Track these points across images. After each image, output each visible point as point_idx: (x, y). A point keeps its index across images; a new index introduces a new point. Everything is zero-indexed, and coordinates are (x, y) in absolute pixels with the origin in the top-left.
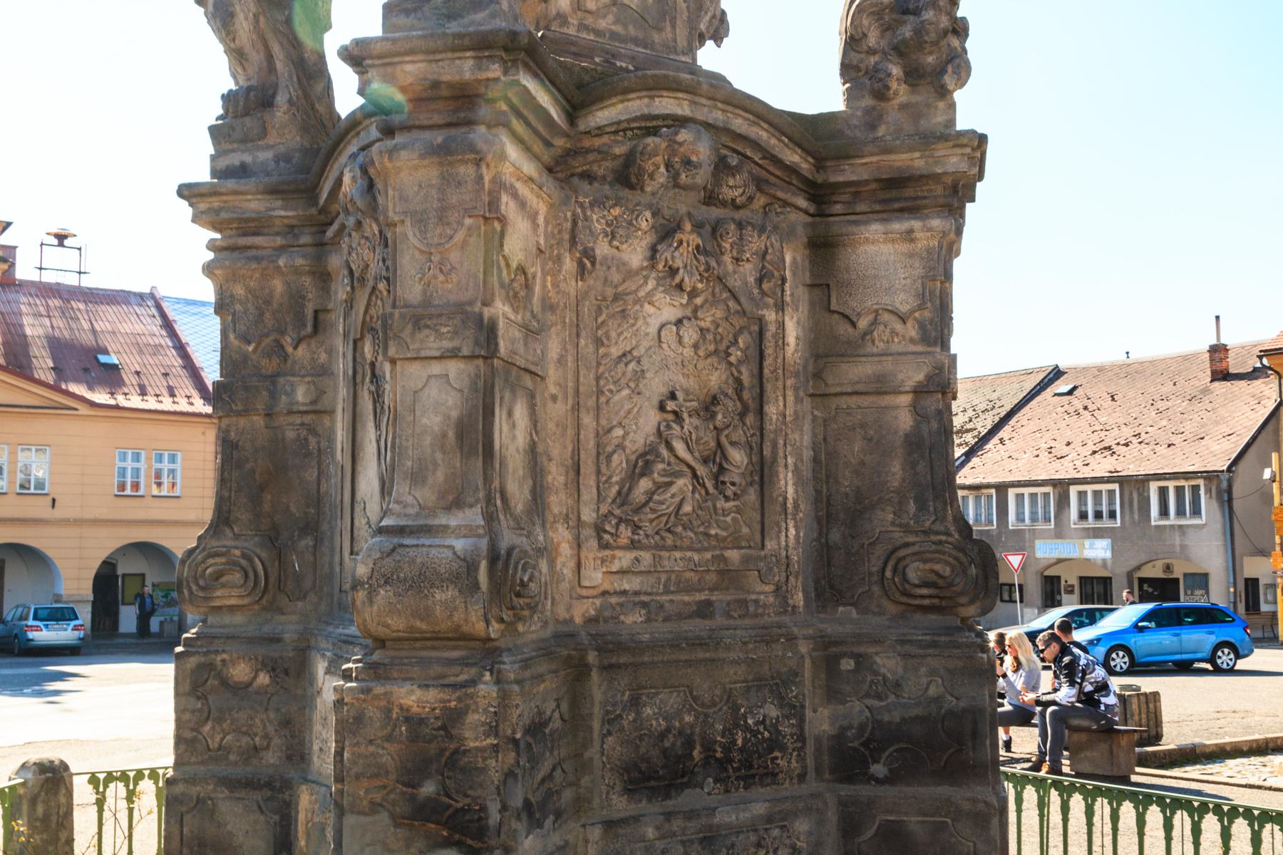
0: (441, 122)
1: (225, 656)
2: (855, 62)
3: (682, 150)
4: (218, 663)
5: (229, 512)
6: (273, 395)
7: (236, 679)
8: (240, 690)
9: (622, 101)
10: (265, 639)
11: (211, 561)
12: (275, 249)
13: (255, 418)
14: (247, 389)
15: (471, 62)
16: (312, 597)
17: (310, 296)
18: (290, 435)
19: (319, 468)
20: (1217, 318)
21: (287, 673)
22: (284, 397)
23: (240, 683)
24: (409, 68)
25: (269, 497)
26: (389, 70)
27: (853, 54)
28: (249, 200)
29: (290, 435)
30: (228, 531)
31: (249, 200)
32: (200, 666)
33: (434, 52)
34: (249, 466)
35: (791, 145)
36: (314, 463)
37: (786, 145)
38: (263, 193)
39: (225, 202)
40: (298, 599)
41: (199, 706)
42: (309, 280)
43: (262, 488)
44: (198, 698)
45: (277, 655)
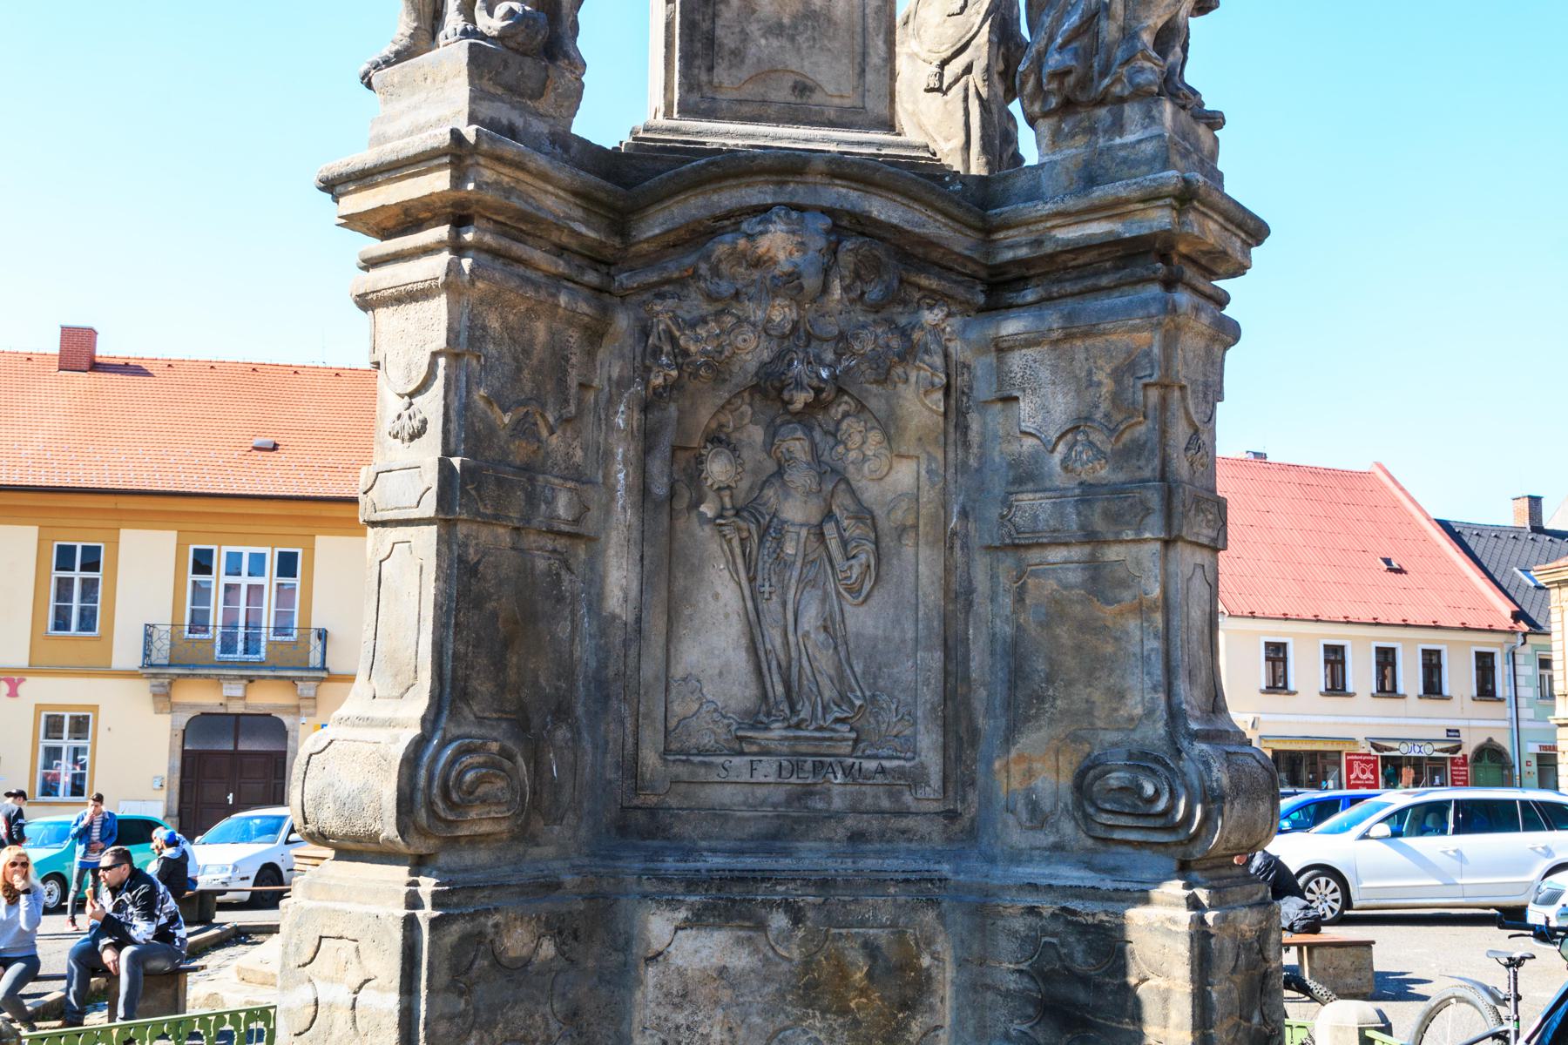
1: (497, 918)
4: (490, 930)
5: (467, 678)
6: (532, 500)
7: (511, 954)
8: (516, 971)
9: (955, 231)
10: (541, 885)
11: (467, 760)
12: (548, 275)
13: (501, 530)
14: (500, 482)
16: (570, 819)
17: (574, 360)
18: (541, 564)
19: (573, 621)
20: (275, 447)
21: (576, 938)
22: (543, 506)
23: (517, 959)
25: (515, 660)
28: (546, 192)
29: (541, 564)
30: (466, 711)
31: (546, 192)
32: (465, 939)
34: (490, 605)
36: (567, 612)
38: (575, 194)
39: (518, 181)
40: (554, 822)
41: (462, 1005)
42: (576, 335)
43: (507, 644)
44: (461, 994)
45: (564, 909)
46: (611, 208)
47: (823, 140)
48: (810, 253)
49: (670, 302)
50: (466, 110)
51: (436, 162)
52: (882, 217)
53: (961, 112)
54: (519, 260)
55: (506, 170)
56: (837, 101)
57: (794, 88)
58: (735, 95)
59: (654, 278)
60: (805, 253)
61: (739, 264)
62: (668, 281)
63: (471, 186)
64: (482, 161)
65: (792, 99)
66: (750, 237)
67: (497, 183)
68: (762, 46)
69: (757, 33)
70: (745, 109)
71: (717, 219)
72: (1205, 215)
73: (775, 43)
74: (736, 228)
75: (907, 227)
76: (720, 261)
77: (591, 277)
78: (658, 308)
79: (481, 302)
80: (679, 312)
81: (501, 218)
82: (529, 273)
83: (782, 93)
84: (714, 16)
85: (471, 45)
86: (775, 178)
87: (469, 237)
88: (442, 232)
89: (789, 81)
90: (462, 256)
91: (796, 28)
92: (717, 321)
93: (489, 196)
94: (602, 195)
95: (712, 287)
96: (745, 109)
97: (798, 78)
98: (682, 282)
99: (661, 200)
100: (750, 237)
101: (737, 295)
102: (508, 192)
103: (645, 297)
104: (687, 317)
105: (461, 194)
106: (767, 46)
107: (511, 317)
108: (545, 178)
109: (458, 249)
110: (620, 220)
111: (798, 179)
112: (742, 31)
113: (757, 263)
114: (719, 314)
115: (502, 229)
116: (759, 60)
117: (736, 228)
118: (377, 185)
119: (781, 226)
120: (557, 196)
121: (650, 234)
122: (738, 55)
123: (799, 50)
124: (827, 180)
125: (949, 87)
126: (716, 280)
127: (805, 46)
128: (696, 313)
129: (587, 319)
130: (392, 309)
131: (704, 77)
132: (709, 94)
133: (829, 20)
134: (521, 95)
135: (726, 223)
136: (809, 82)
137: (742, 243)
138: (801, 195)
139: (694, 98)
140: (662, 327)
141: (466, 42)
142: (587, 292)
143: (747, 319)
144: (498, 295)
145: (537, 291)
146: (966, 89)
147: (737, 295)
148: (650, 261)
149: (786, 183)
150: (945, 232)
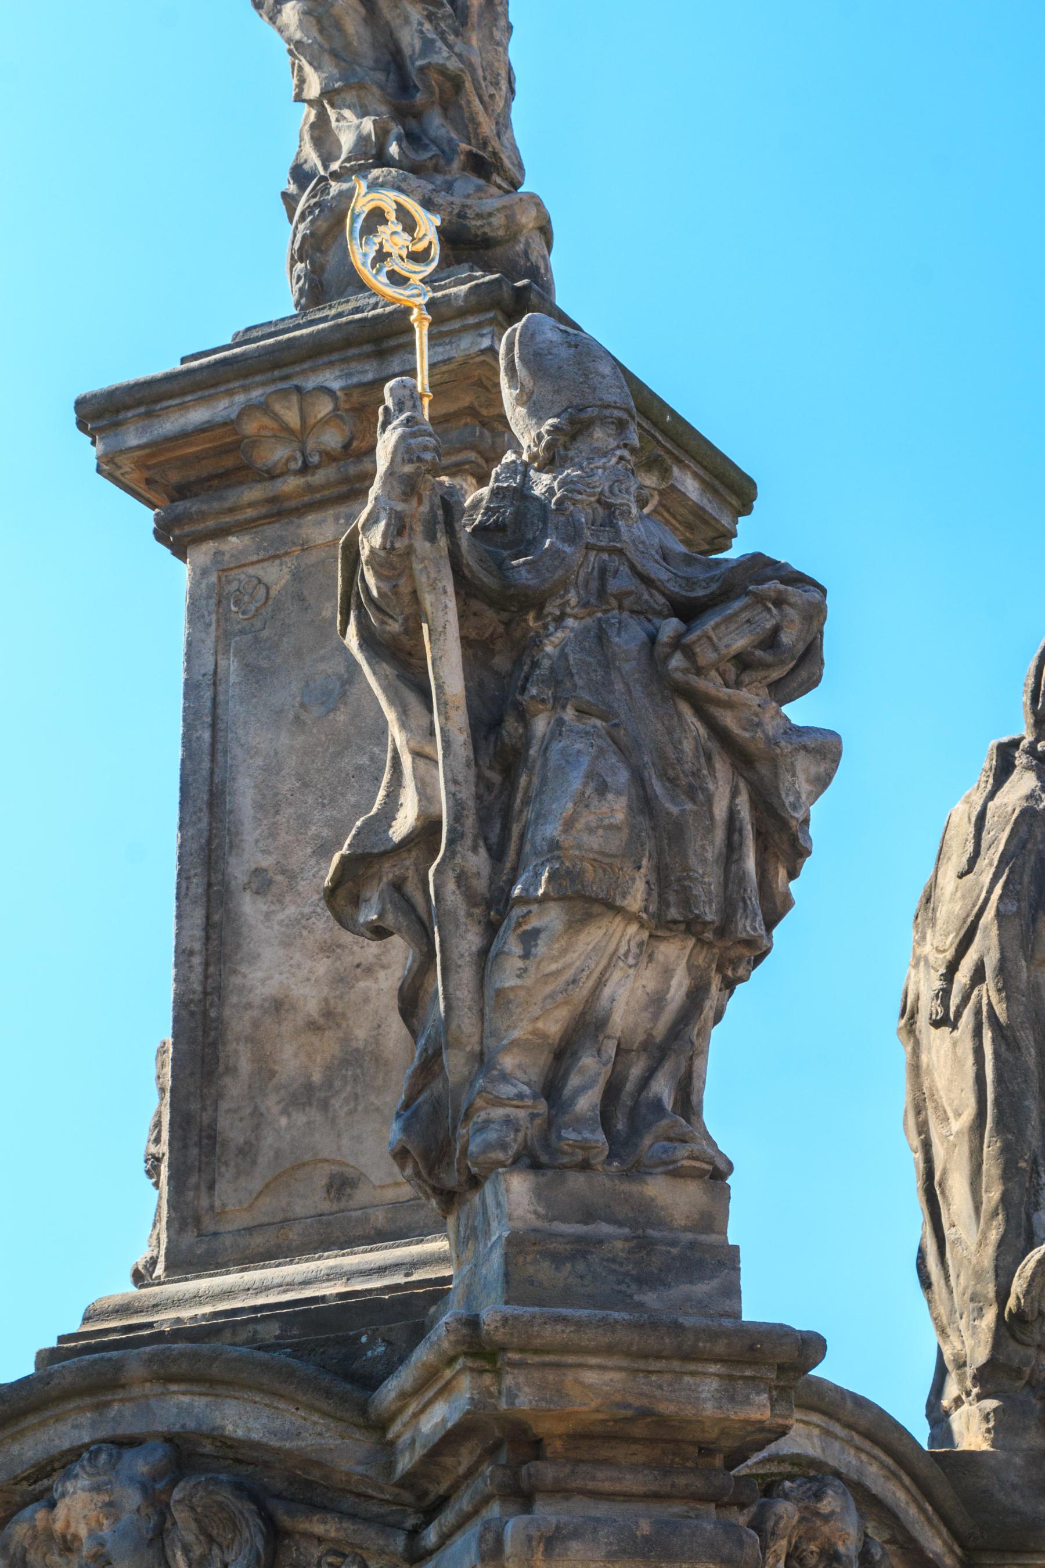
0: (637, 1488)
2: (1016, 1363)
3: (826, 1529)
15: (714, 1384)
24: (591, 1377)
26: (551, 1376)
27: (1012, 1345)
33: (645, 1356)
35: (936, 1519)
37: (929, 1520)
47: (330, 1277)
48: (125, 1517)
52: (240, 1433)
53: (970, 1059)
57: (329, 1188)
58: (245, 1220)
60: (117, 1519)
68: (284, 1127)
69: (276, 1110)
72: (557, 1366)
73: (300, 1119)
75: (275, 1443)
86: (88, 1400)
89: (320, 1177)
91: (331, 1086)
96: (258, 1241)
97: (335, 1169)
106: (289, 1127)
111: (120, 1394)
116: (278, 1154)
119: (84, 1482)
122: (248, 1151)
124: (158, 1388)
125: (958, 1014)
127: (342, 1113)
132: (212, 1228)
136: (349, 1172)
138: (123, 1416)
146: (978, 1012)
149: (107, 1404)
150: (331, 1440)
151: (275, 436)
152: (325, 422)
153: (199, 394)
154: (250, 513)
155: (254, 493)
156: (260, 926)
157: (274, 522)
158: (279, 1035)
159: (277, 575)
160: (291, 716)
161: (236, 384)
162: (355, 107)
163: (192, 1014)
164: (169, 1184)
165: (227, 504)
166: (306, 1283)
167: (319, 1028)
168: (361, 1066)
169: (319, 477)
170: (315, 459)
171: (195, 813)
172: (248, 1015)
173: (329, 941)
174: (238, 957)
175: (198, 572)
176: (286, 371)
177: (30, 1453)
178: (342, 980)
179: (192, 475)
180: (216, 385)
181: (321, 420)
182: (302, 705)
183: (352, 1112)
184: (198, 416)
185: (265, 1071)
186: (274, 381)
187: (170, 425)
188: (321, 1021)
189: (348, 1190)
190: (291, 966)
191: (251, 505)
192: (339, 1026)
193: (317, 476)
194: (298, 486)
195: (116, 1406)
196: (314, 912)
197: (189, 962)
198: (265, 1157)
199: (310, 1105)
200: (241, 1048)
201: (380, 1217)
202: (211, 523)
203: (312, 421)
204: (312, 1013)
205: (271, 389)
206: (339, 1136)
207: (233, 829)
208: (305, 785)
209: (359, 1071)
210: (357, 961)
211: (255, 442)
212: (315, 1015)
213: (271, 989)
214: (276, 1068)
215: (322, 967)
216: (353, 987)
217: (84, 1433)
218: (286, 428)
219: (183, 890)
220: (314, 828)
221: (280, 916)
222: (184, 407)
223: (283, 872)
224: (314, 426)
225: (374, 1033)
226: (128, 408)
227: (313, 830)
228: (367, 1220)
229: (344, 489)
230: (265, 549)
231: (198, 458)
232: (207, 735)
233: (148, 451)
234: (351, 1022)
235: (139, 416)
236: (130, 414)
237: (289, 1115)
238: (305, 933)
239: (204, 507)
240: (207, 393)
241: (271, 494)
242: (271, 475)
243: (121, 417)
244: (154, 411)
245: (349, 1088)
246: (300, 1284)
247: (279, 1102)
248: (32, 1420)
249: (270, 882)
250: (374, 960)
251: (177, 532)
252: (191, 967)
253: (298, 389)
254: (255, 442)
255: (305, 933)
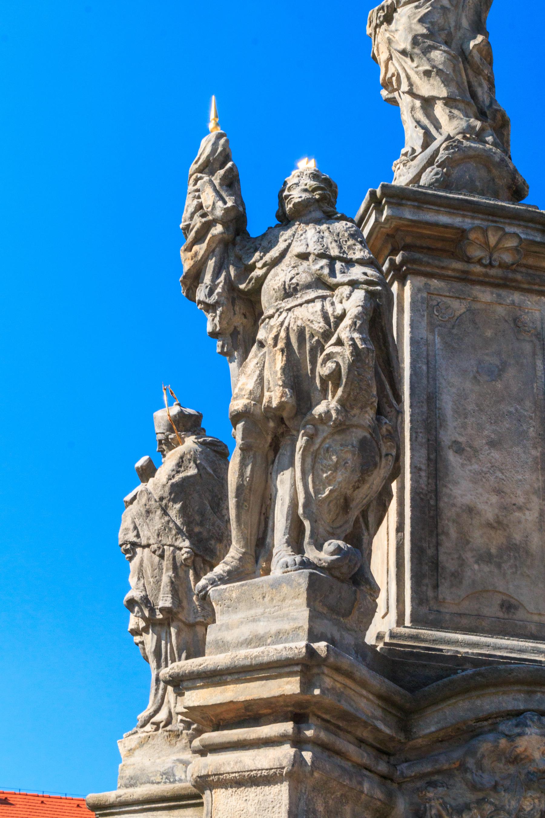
28: (361, 695)
31: (361, 695)
38: (380, 697)
39: (345, 686)
46: (400, 708)
49: (441, 790)
50: (306, 627)
51: (287, 670)
54: (339, 753)
55: (340, 678)
56: (536, 618)
57: (502, 606)
59: (428, 768)
61: (499, 760)
62: (439, 772)
63: (317, 692)
64: (326, 670)
65: (501, 614)
66: (510, 738)
67: (333, 689)
68: (476, 571)
69: (472, 560)
70: (464, 621)
71: (478, 720)
73: (486, 569)
74: (494, 728)
76: (483, 756)
77: (382, 767)
78: (430, 795)
79: (314, 789)
80: (447, 799)
81: (327, 717)
82: (344, 763)
83: (492, 610)
84: (438, 545)
85: (311, 574)
86: (526, 688)
87: (309, 733)
88: (288, 727)
89: (497, 599)
90: (301, 749)
91: (502, 557)
92: (479, 809)
93: (329, 700)
94: (397, 698)
95: (477, 779)
96: (464, 621)
97: (505, 598)
98: (448, 773)
99: (435, 703)
100: (510, 738)
101: (495, 788)
102: (340, 695)
103: (419, 784)
104: (454, 804)
105: (307, 697)
107: (331, 802)
108: (363, 684)
109: (298, 742)
110: (405, 717)
112: (460, 558)
113: (516, 760)
114: (480, 802)
115: (326, 724)
116: (474, 582)
117: (494, 728)
118: (226, 683)
120: (368, 699)
121: (427, 731)
122: (457, 577)
123: (504, 575)
126: (480, 772)
127: (509, 572)
128: (461, 801)
129: (379, 803)
130: (230, 790)
131: (430, 593)
132: (435, 608)
133: (527, 552)
134: (338, 614)
135: (485, 723)
136: (513, 601)
137: (503, 742)
139: (424, 610)
140: (434, 812)
141: (307, 571)
142: (376, 778)
143: (502, 808)
144: (326, 783)
145: (351, 780)
147: (495, 788)
148: (423, 754)
149: (535, 692)
151: (480, 245)
152: (507, 249)
153: (448, 210)
154: (450, 273)
155: (458, 265)
156: (458, 468)
157: (458, 282)
158: (471, 524)
159: (459, 307)
160: (472, 375)
161: (469, 214)
162: (463, 111)
163: (422, 499)
164: (411, 579)
165: (442, 265)
166: (500, 648)
167: (494, 528)
168: (518, 553)
169: (493, 272)
170: (496, 264)
171: (419, 402)
172: (453, 510)
173: (498, 488)
174: (447, 479)
175: (416, 289)
176: (497, 219)
177: (488, 707)
178: (505, 508)
179: (418, 243)
180: (457, 209)
181: (506, 247)
182: (478, 372)
183: (514, 573)
184: (444, 219)
185: (464, 541)
186: (488, 220)
187: (429, 216)
188: (495, 525)
189: (513, 610)
190: (477, 493)
191: (454, 270)
192: (505, 530)
193: (492, 271)
194: (482, 272)
195: (539, 695)
196: (489, 472)
197: (419, 473)
198: (466, 582)
199: (491, 563)
200: (450, 524)
201: (533, 628)
202: (428, 269)
203: (501, 246)
204: (490, 519)
205: (490, 224)
206: (507, 583)
207: (441, 417)
208: (481, 410)
209: (517, 555)
210: (513, 502)
211: (471, 243)
212: (492, 521)
213: (467, 499)
214: (470, 540)
215: (494, 499)
216: (512, 513)
217: (520, 704)
218: (487, 243)
219: (414, 438)
220: (486, 432)
221: (469, 467)
222: (438, 212)
223: (471, 447)
224: (501, 248)
225: (525, 539)
226: (408, 199)
227: (486, 433)
228: (526, 627)
229: (501, 282)
230: (453, 292)
231: (429, 237)
232: (424, 367)
233: (409, 223)
234: (512, 531)
235: (414, 206)
236: (409, 203)
237: (479, 565)
238: (484, 480)
239: (430, 261)
240: (452, 211)
241: (466, 269)
242: (469, 260)
243: (404, 202)
244: (423, 207)
245: (512, 561)
246: (518, 651)
247: (473, 557)
248: (492, 690)
249: (463, 450)
250: (522, 505)
251: (409, 266)
252: (420, 476)
253: (503, 229)
254: (471, 243)
255: (484, 480)
